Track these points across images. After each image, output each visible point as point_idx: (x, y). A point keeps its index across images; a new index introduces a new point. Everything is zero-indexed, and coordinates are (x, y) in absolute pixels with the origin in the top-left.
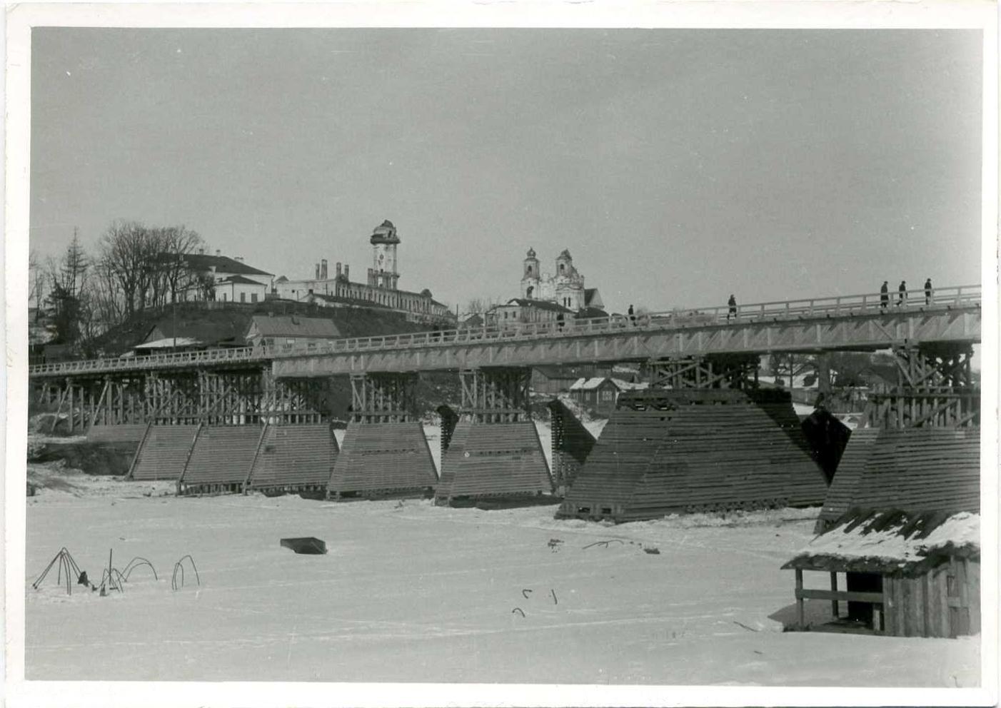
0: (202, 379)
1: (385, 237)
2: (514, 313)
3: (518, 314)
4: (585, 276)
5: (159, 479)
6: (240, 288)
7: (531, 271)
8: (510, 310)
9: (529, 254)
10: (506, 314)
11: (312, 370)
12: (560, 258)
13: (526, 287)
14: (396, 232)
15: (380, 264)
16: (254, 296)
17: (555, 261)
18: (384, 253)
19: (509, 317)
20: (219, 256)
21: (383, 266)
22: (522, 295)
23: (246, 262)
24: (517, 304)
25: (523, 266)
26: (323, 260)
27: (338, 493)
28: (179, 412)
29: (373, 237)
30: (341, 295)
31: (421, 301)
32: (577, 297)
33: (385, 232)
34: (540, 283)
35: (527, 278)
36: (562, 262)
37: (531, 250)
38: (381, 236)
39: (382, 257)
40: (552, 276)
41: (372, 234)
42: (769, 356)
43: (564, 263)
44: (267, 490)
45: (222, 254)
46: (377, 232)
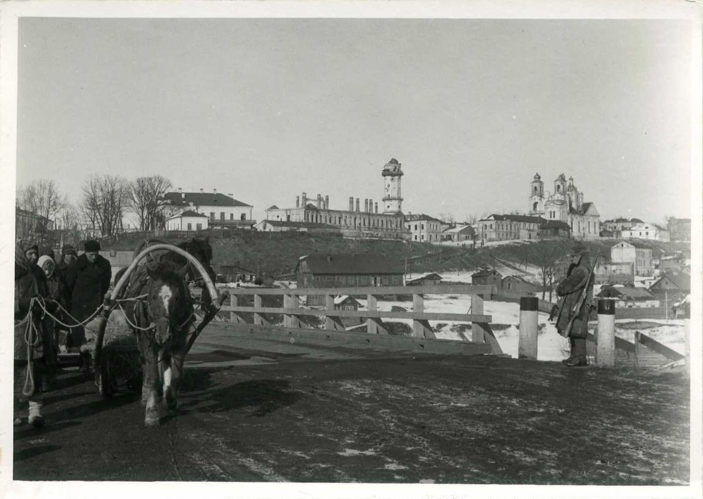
1: (393, 171)
2: (491, 225)
3: (494, 227)
4: (583, 193)
6: (187, 220)
7: (538, 190)
8: (488, 223)
10: (486, 226)
13: (533, 202)
14: (400, 167)
15: (388, 191)
16: (199, 226)
17: (553, 183)
18: (390, 183)
19: (488, 228)
20: (215, 193)
21: (390, 193)
22: (265, 218)
23: (235, 198)
25: (531, 187)
26: (304, 193)
29: (384, 171)
30: (310, 221)
31: (393, 220)
32: (560, 211)
33: (391, 168)
35: (534, 196)
36: (559, 183)
37: (537, 174)
38: (388, 170)
39: (389, 186)
40: (551, 194)
41: (383, 169)
43: (560, 184)
45: (218, 192)
46: (386, 168)
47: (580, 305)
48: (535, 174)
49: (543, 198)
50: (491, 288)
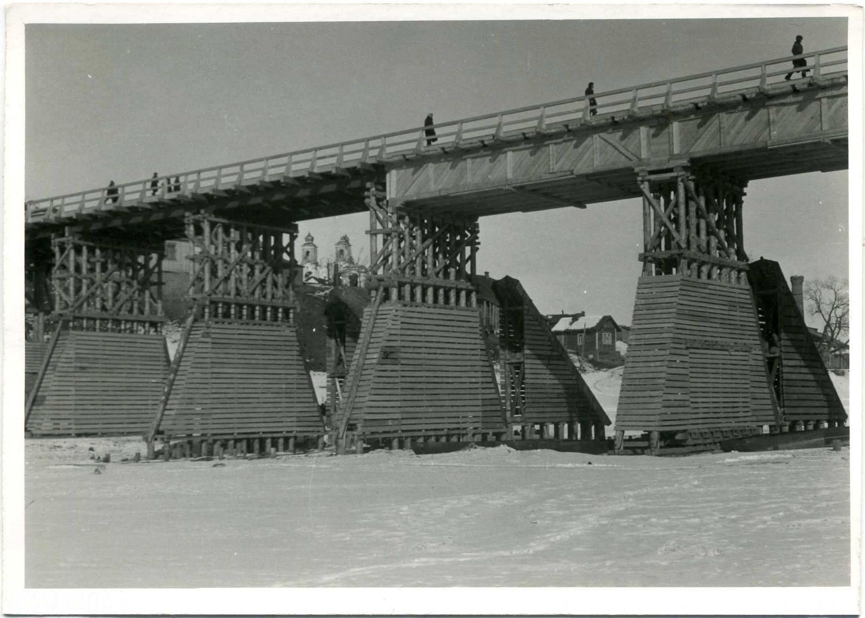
0: (192, 228)
5: (79, 435)
9: (306, 239)
11: (510, 176)
12: (339, 243)
24: (316, 282)
27: (655, 436)
28: (115, 309)
34: (318, 268)
37: (309, 235)
42: (583, 334)
44: (414, 439)
47: (617, 520)
48: (307, 235)
49: (320, 266)
50: (772, 138)
